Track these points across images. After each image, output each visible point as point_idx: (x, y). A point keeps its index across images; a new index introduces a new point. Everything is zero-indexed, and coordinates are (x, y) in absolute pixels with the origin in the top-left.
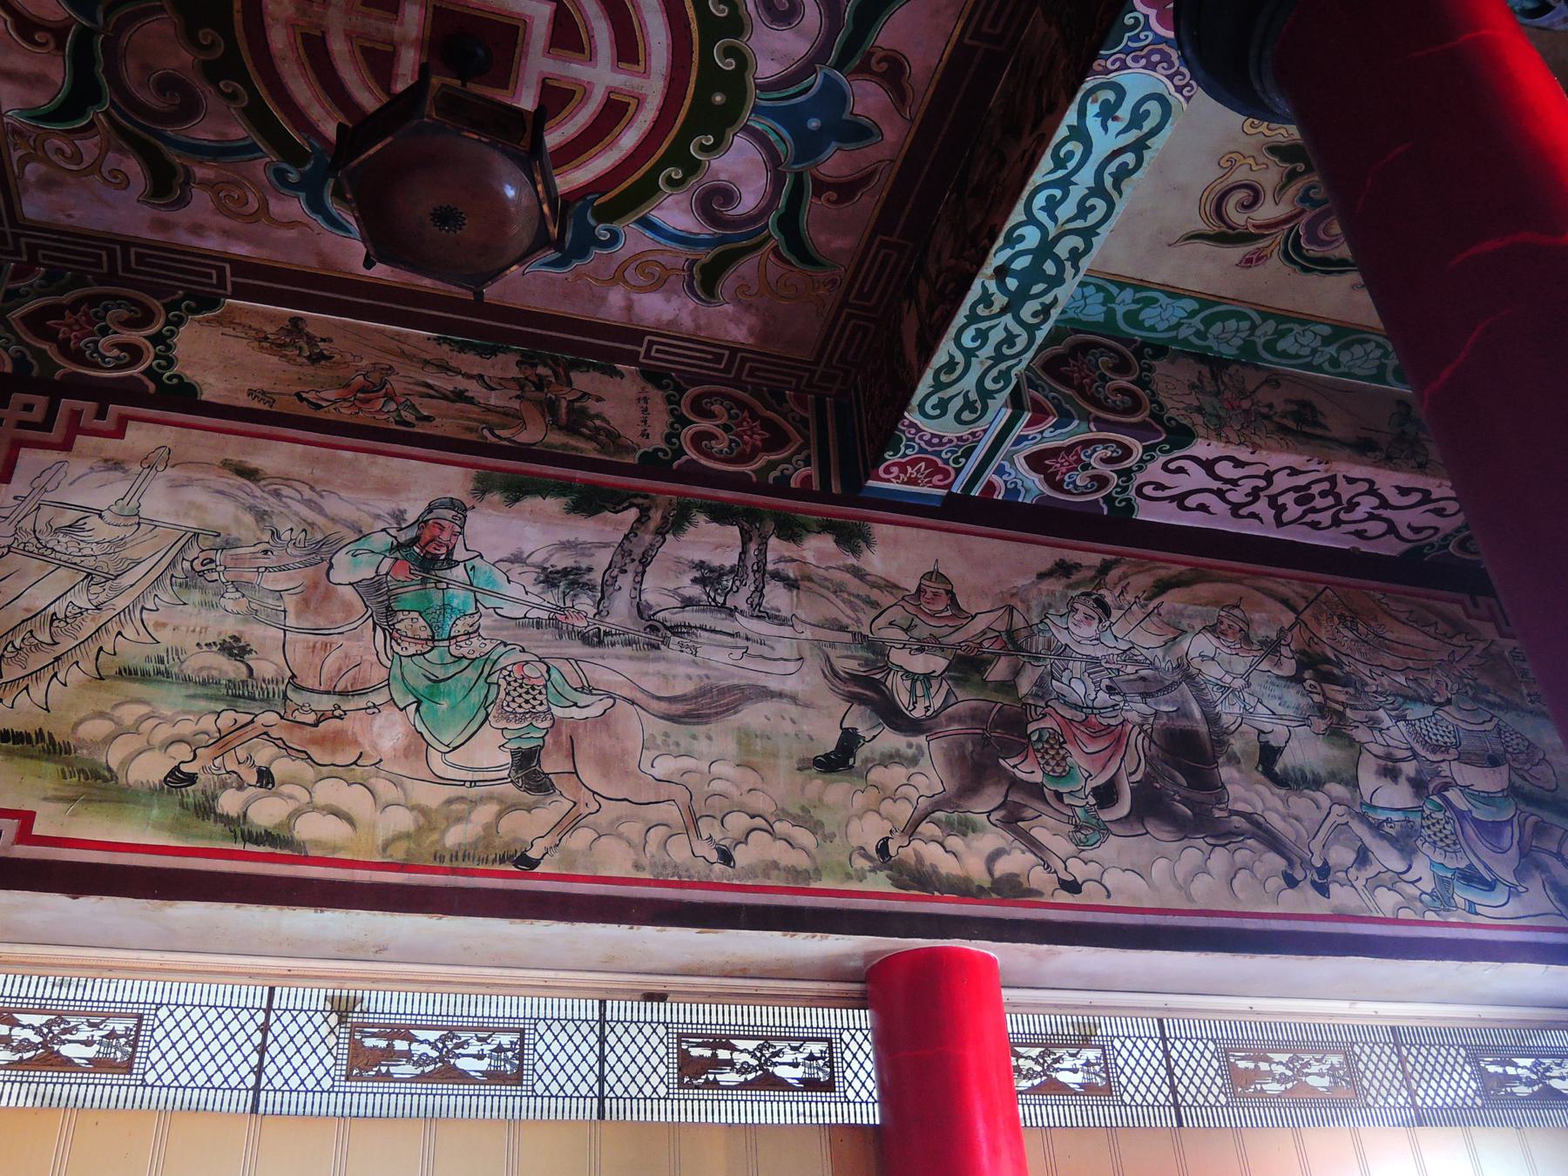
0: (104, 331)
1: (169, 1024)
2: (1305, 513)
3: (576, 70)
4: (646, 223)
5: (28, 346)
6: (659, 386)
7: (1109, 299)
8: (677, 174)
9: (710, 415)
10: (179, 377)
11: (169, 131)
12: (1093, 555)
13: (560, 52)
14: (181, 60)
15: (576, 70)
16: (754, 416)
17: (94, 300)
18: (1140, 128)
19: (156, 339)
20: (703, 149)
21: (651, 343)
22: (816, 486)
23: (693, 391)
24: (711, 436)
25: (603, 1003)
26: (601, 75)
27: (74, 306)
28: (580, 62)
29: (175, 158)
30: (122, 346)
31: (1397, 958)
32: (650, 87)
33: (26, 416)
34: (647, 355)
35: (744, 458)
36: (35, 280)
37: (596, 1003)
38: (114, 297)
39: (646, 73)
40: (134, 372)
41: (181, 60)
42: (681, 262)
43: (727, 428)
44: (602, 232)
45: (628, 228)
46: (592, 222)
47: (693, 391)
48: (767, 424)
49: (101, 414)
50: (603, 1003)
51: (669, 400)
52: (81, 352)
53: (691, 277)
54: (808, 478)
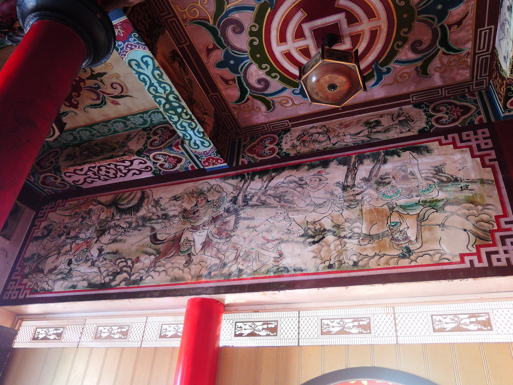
0: (266, 147)
1: (284, 322)
2: (105, 175)
3: (357, 29)
4: (397, 62)
5: (250, 157)
6: (420, 108)
7: (72, 134)
8: (400, 43)
9: (439, 111)
10: (284, 153)
11: (266, 92)
12: (110, 196)
13: (351, 25)
14: (262, 74)
15: (357, 29)
16: (456, 106)
17: (262, 140)
18: (138, 68)
19: (431, 116)
20: (405, 33)
21: (413, 96)
22: (485, 121)
23: (432, 106)
24: (442, 118)
25: (393, 308)
26: (292, 46)
27: (258, 144)
28: (360, 25)
29: (269, 98)
30: (270, 150)
31: (42, 303)
32: (278, 50)
33: (485, 136)
34: (413, 101)
35: (454, 121)
36: (248, 140)
37: (392, 308)
38: (266, 138)
39: (379, 19)
40: (275, 155)
41: (262, 74)
42: (413, 69)
43: (447, 113)
44: (384, 69)
45: (392, 65)
46: (380, 68)
47: (432, 106)
48: (461, 107)
49: (446, 138)
50: (393, 308)
51: (425, 111)
52: (261, 154)
53: (273, 104)
54: (481, 119)
